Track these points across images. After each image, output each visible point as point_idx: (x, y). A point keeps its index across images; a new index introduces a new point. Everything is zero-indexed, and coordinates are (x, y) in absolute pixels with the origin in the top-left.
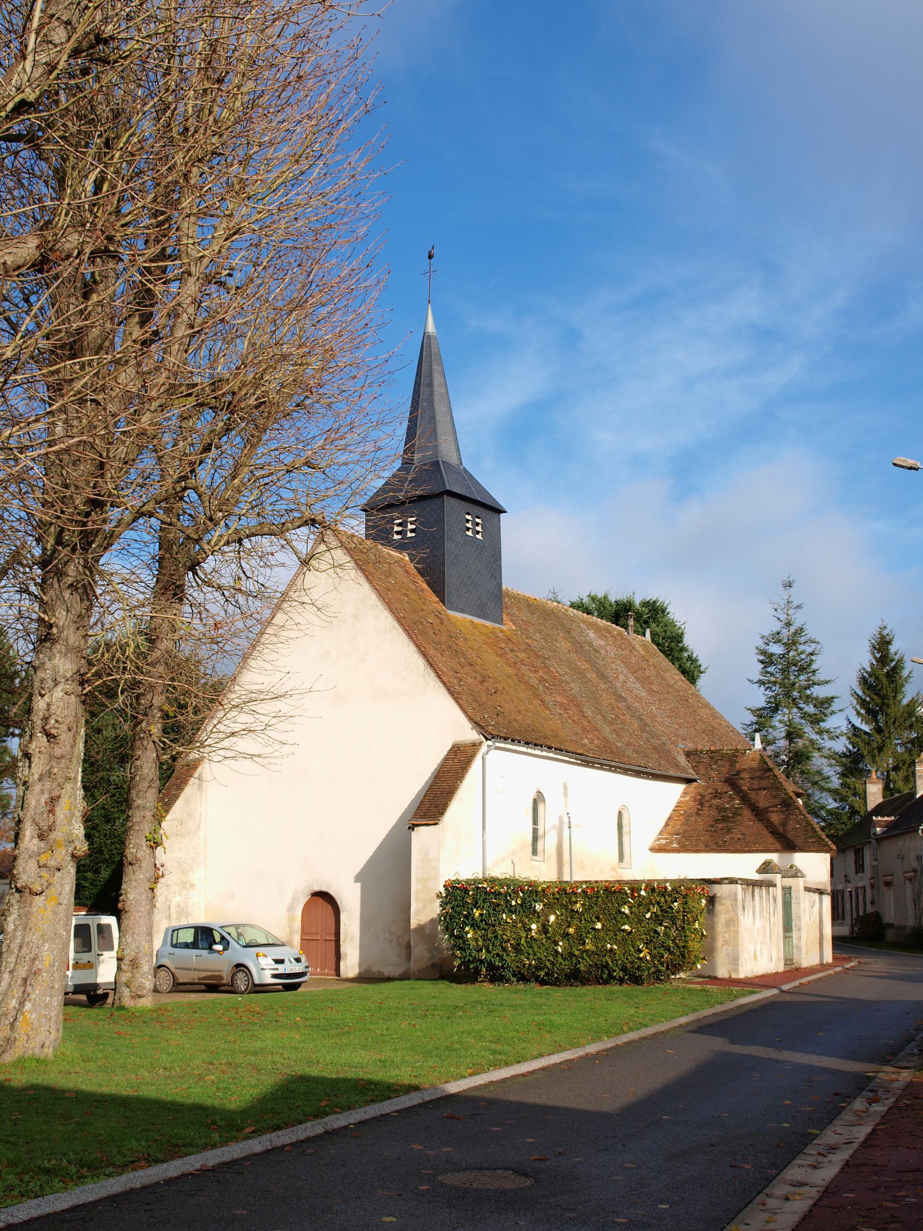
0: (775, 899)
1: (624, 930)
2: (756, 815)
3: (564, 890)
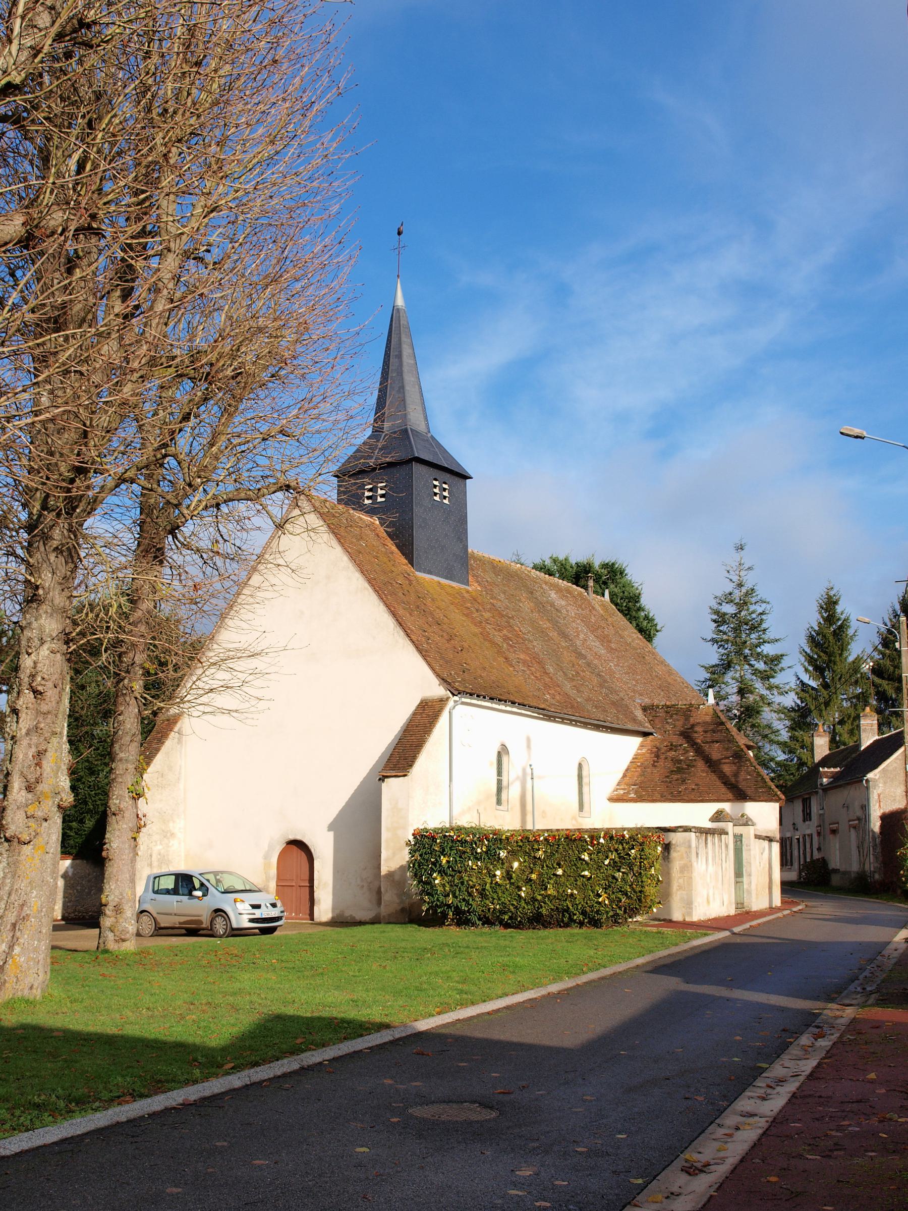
0: (727, 846)
1: (583, 876)
2: (709, 767)
3: (527, 838)
